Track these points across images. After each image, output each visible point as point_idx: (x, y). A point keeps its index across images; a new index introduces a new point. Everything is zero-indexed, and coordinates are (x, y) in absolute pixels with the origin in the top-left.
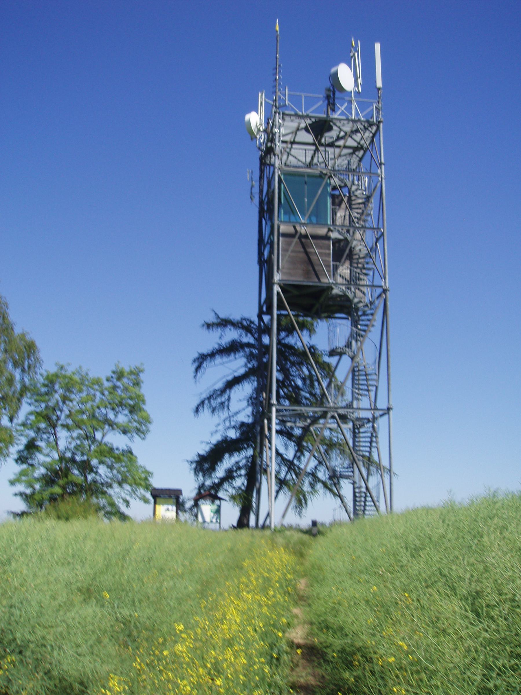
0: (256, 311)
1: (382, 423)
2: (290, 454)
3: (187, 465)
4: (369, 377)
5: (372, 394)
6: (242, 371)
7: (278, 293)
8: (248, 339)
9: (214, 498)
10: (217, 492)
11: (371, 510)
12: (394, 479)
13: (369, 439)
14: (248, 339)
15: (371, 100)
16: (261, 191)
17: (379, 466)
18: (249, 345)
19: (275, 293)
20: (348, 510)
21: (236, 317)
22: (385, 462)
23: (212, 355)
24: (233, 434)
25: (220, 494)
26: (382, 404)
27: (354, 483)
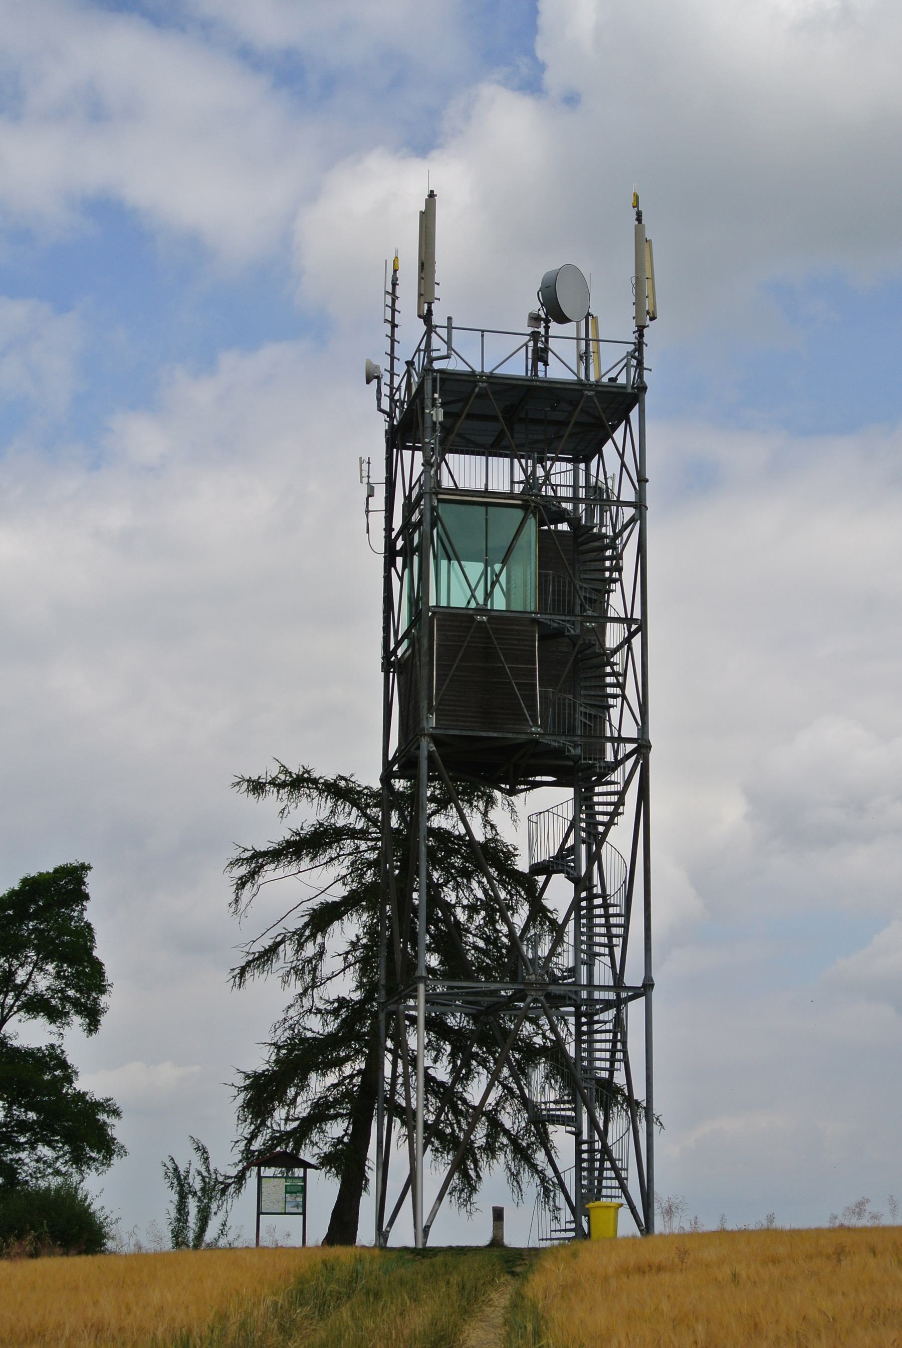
0: (379, 770)
1: (635, 1009)
2: (442, 1072)
3: (86, 1090)
4: (612, 910)
5: (618, 951)
6: (339, 892)
7: (430, 756)
8: (349, 817)
9: (291, 1161)
10: (297, 1148)
11: (611, 1188)
12: (656, 1128)
13: (608, 1046)
14: (349, 817)
15: (608, 426)
16: (389, 528)
17: (631, 1103)
18: (353, 834)
19: (424, 753)
20: (567, 841)
21: (326, 772)
22: (639, 1094)
23: (276, 855)
24: (316, 1026)
25: (307, 1154)
26: (633, 977)
27: (578, 1134)
